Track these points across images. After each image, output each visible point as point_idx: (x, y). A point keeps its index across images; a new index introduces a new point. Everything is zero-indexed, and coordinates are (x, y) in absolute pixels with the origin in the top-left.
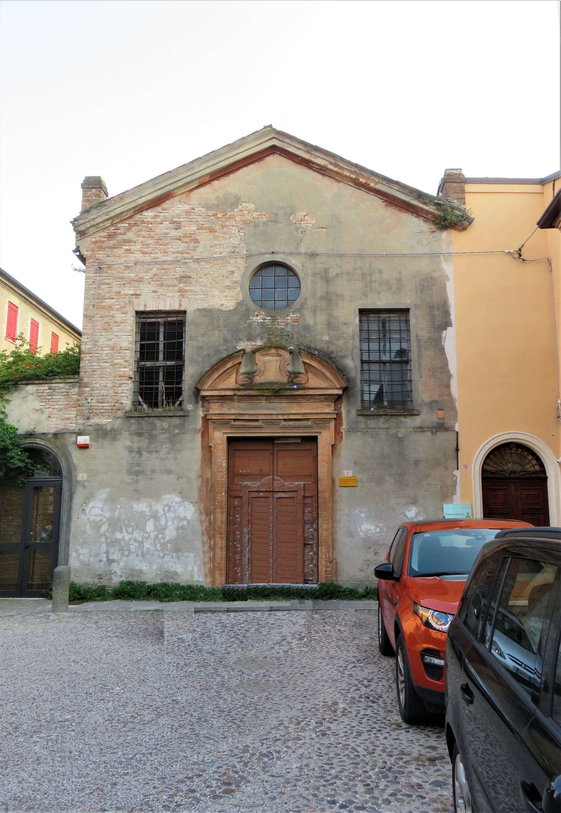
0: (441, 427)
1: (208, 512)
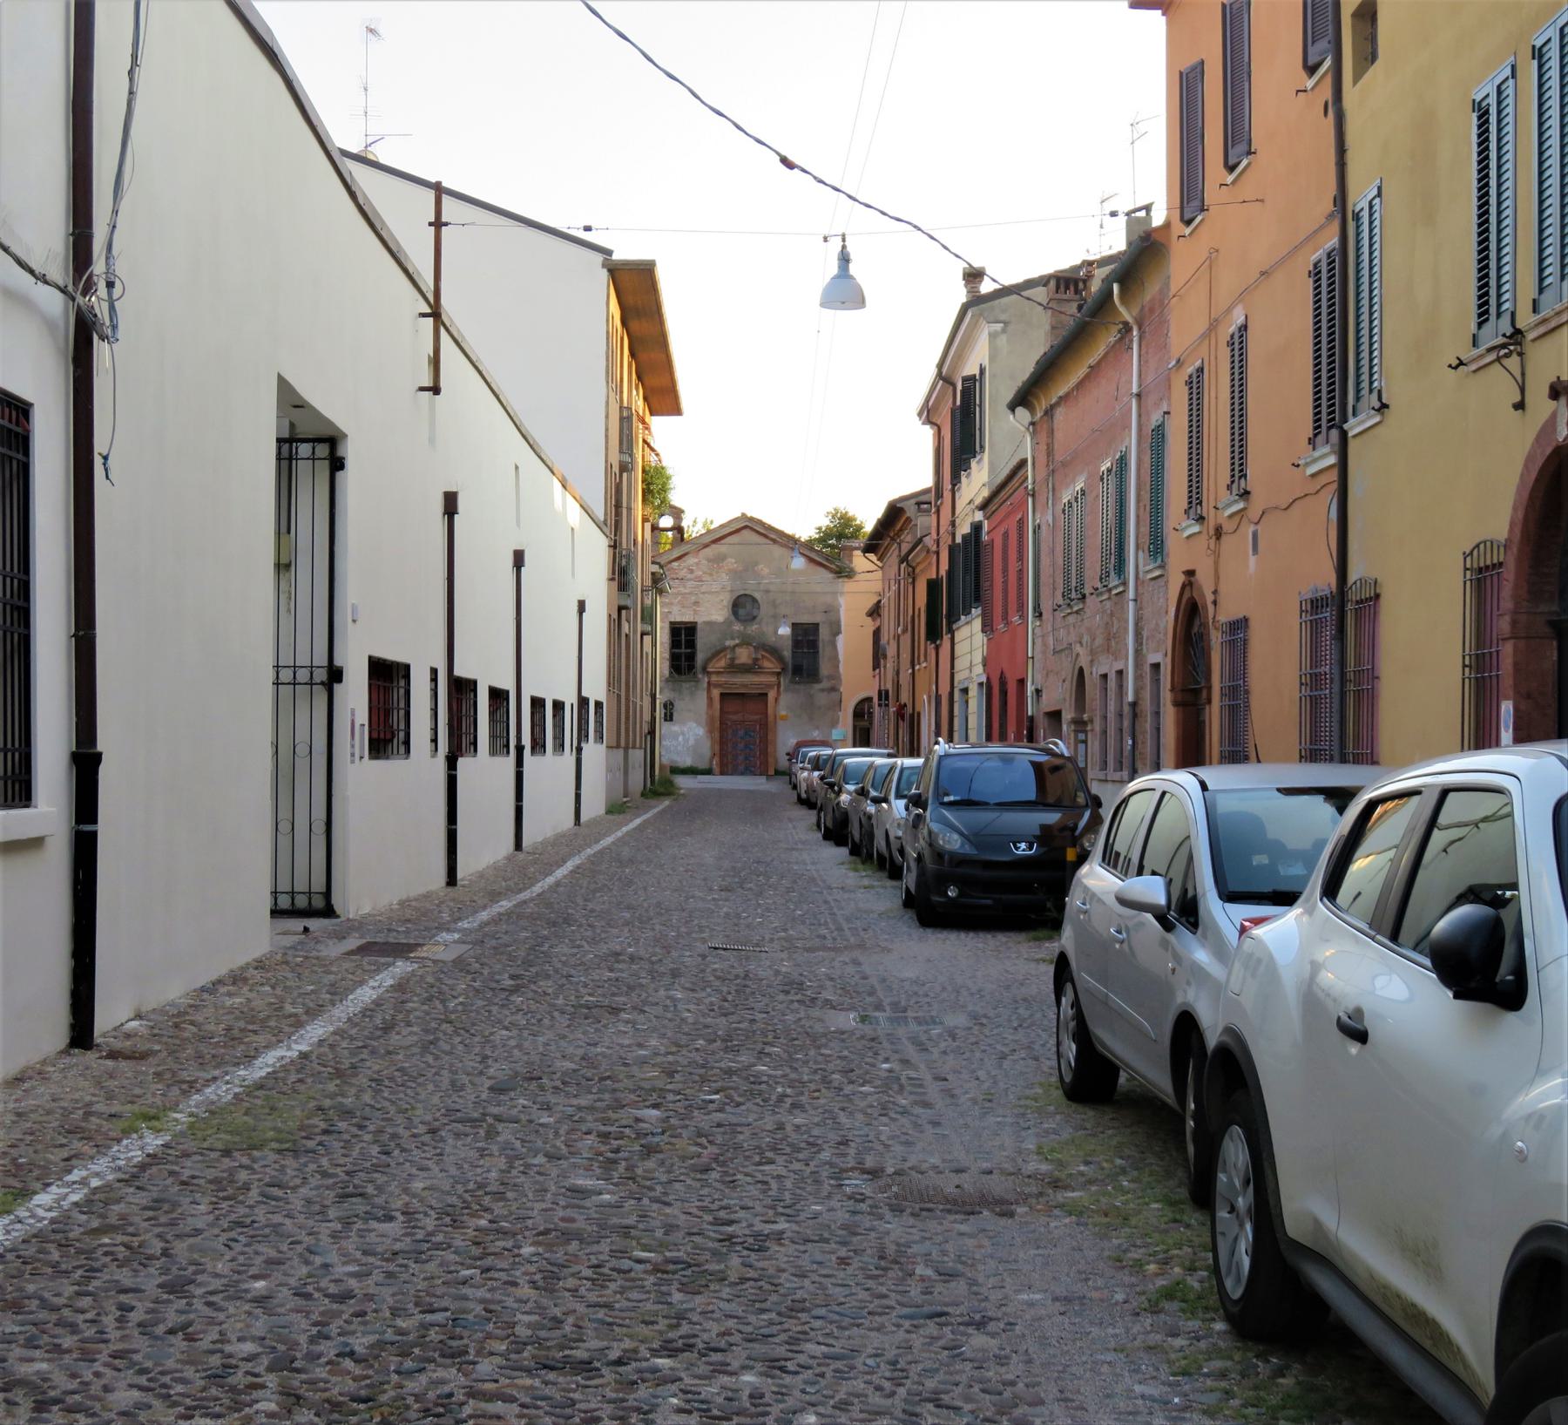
0: (834, 689)
1: (710, 731)
